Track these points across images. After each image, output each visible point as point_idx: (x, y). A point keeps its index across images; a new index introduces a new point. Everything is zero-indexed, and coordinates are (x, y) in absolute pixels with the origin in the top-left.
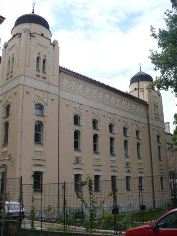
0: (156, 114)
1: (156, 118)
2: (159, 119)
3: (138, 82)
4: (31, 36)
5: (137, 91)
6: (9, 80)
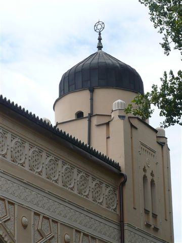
0: (147, 212)
1: (148, 226)
2: (156, 229)
3: (92, 91)
5: (84, 123)
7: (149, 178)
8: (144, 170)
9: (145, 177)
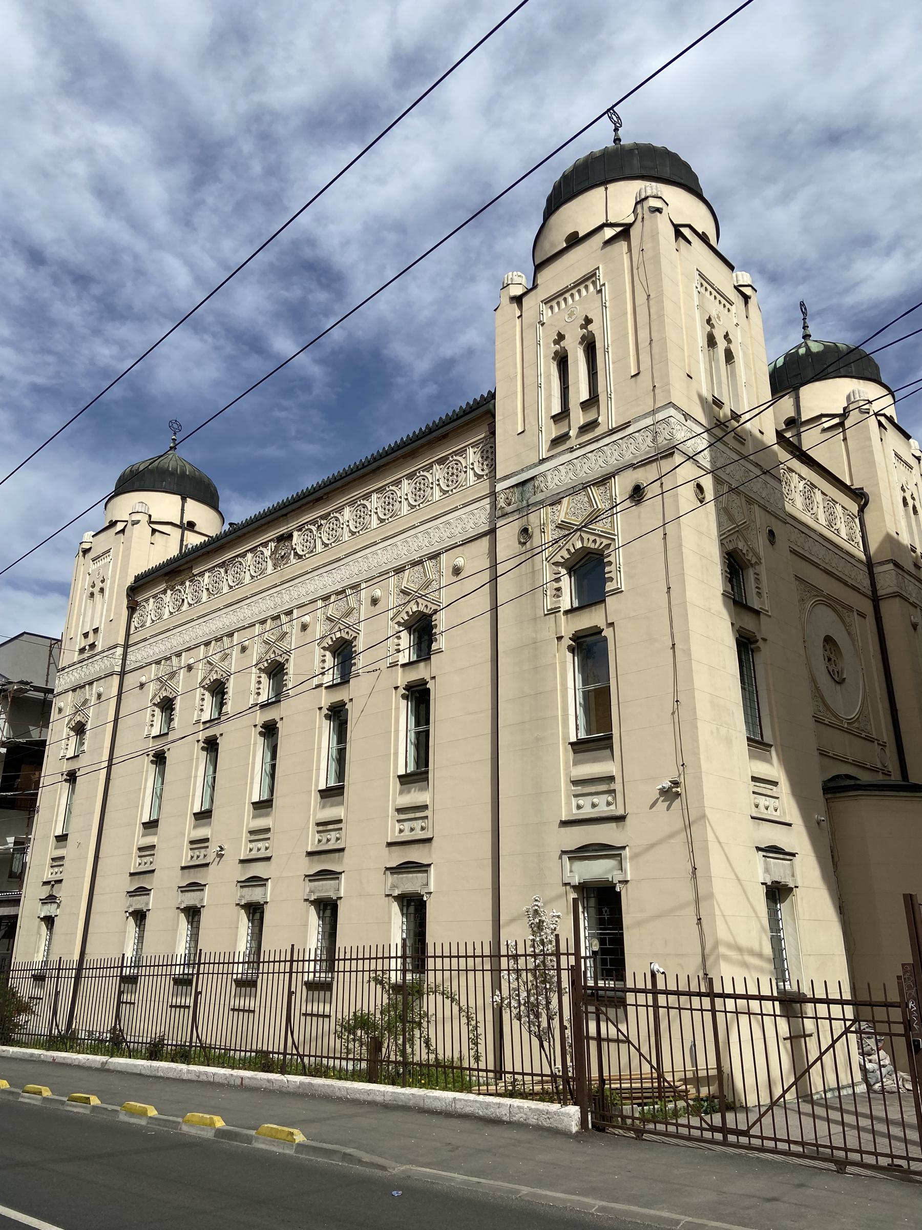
4: (154, 531)
6: (86, 655)
7: (910, 502)
8: (904, 490)
9: (904, 499)
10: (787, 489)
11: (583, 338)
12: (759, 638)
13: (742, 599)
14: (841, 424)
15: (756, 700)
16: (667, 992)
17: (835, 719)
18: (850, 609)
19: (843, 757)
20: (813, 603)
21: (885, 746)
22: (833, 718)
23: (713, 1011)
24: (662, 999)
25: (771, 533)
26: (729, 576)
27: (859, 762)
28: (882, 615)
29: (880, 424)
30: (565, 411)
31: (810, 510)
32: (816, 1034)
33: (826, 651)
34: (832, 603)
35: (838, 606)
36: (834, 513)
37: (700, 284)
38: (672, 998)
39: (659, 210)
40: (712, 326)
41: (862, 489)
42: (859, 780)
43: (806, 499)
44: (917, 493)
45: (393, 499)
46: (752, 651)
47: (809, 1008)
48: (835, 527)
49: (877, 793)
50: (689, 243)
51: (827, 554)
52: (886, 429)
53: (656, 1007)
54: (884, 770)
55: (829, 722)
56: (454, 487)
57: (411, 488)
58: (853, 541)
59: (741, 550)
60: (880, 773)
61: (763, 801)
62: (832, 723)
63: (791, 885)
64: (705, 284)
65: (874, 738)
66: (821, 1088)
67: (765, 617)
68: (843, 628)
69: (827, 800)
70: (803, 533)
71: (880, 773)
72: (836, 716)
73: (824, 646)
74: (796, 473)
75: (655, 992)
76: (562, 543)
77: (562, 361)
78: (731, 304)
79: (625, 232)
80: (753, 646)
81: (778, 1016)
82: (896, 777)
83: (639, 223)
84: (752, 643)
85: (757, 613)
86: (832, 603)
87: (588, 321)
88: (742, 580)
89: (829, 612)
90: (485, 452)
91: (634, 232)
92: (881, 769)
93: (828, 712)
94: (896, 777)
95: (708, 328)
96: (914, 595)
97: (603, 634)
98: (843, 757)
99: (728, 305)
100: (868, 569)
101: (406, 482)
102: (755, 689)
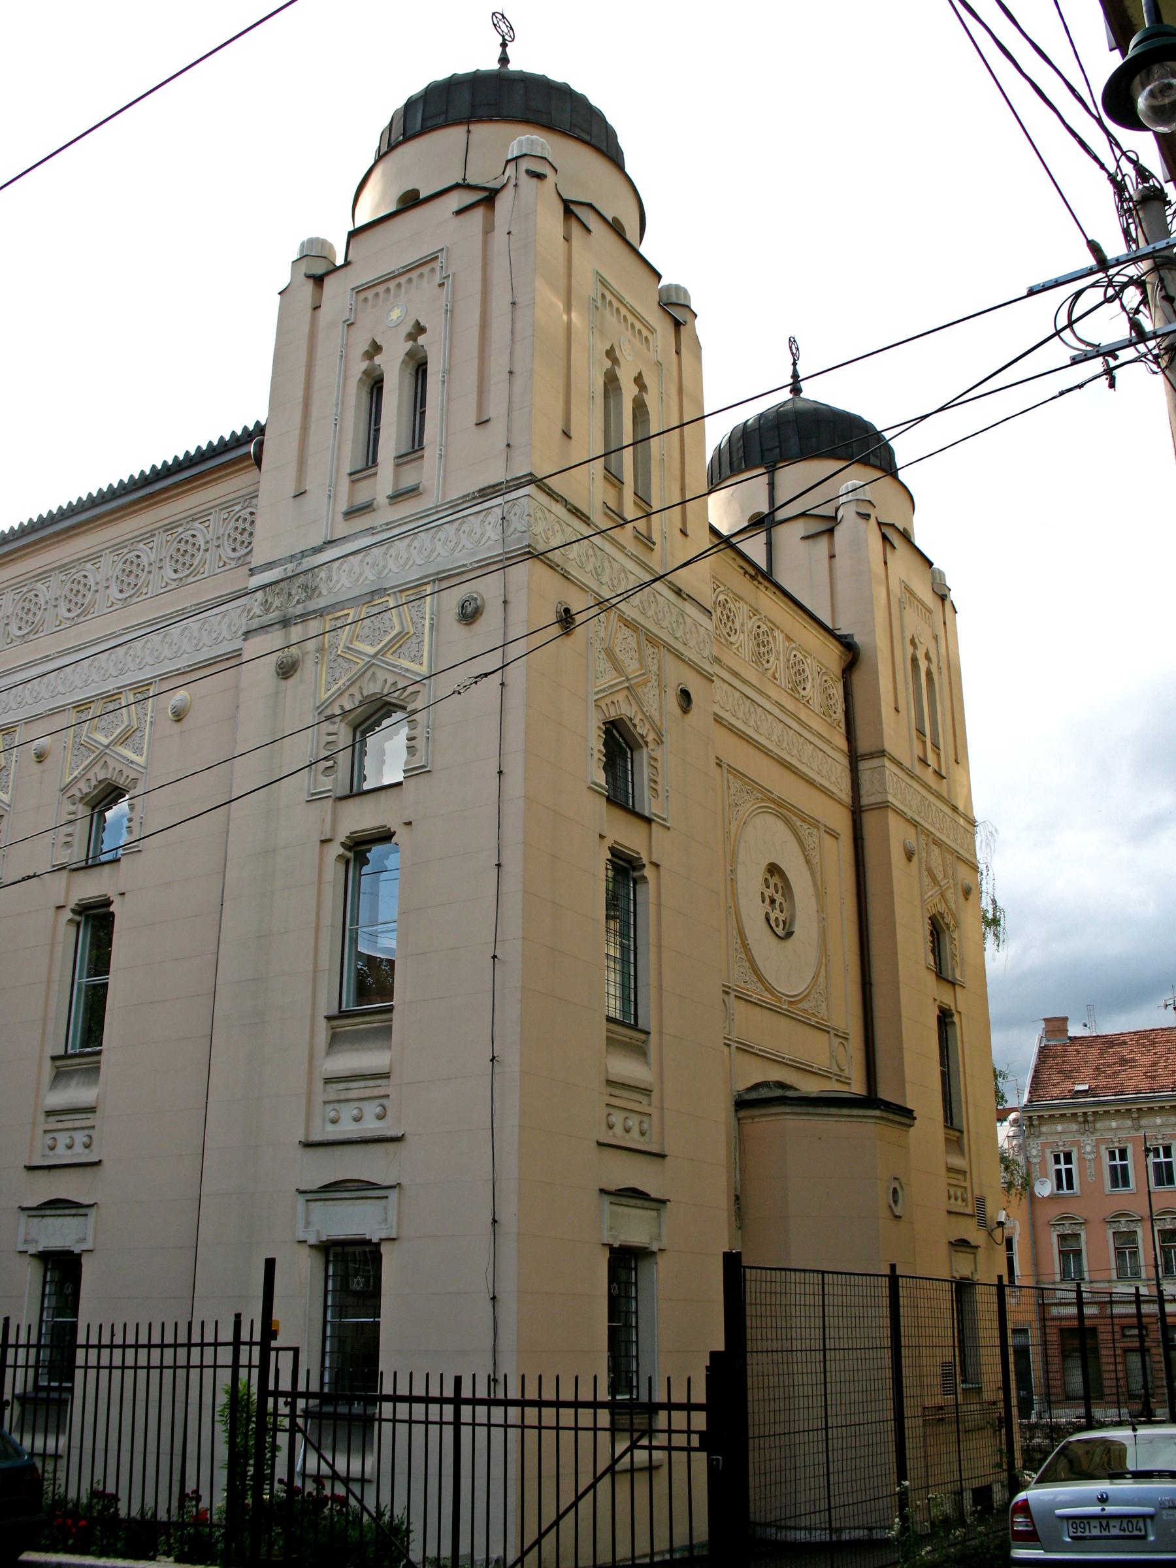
6: (918, 769)
9: (914, 660)
10: (728, 627)
11: (410, 354)
12: (645, 861)
13: (627, 797)
14: (831, 531)
15: (632, 961)
16: (474, 1402)
17: (769, 996)
18: (814, 823)
19: (776, 1055)
20: (753, 811)
21: (846, 1039)
22: (766, 994)
23: (457, 1423)
24: (466, 1410)
25: (685, 696)
26: (604, 759)
27: (803, 1064)
28: (865, 837)
29: (885, 538)
30: (417, 451)
31: (764, 662)
32: (666, 1467)
33: (768, 887)
34: (782, 810)
35: (794, 818)
36: (803, 670)
37: (599, 295)
38: (481, 1410)
39: (540, 177)
40: (615, 361)
41: (851, 636)
42: (796, 1089)
43: (758, 644)
44: (935, 651)
45: (85, 585)
46: (635, 883)
47: (387, 1407)
48: (803, 693)
49: (811, 1110)
50: (588, 231)
51: (785, 733)
52: (894, 547)
53: (457, 1423)
54: (840, 1076)
55: (759, 1000)
56: (185, 574)
57: (117, 570)
58: (831, 716)
59: (631, 719)
60: (834, 1080)
61: (617, 1118)
62: (763, 1001)
63: (655, 1248)
64: (609, 297)
65: (829, 1027)
66: (666, 1546)
67: (660, 829)
68: (800, 854)
69: (739, 1119)
70: (748, 697)
71: (834, 1080)
72: (769, 989)
73: (766, 880)
74: (746, 603)
75: (457, 1401)
76: (344, 684)
77: (375, 386)
78: (652, 330)
79: (489, 198)
80: (636, 874)
81: (650, 1442)
82: (858, 1088)
83: (510, 189)
84: (634, 869)
85: (648, 821)
86: (782, 810)
87: (419, 329)
88: (630, 768)
89: (780, 826)
90: (241, 520)
91: (503, 202)
92: (836, 1075)
93: (759, 984)
94: (858, 1088)
95: (608, 364)
96: (915, 808)
97: (112, 909)
98: (776, 1055)
99: (645, 333)
100: (851, 762)
101: (111, 558)
102: (632, 943)
